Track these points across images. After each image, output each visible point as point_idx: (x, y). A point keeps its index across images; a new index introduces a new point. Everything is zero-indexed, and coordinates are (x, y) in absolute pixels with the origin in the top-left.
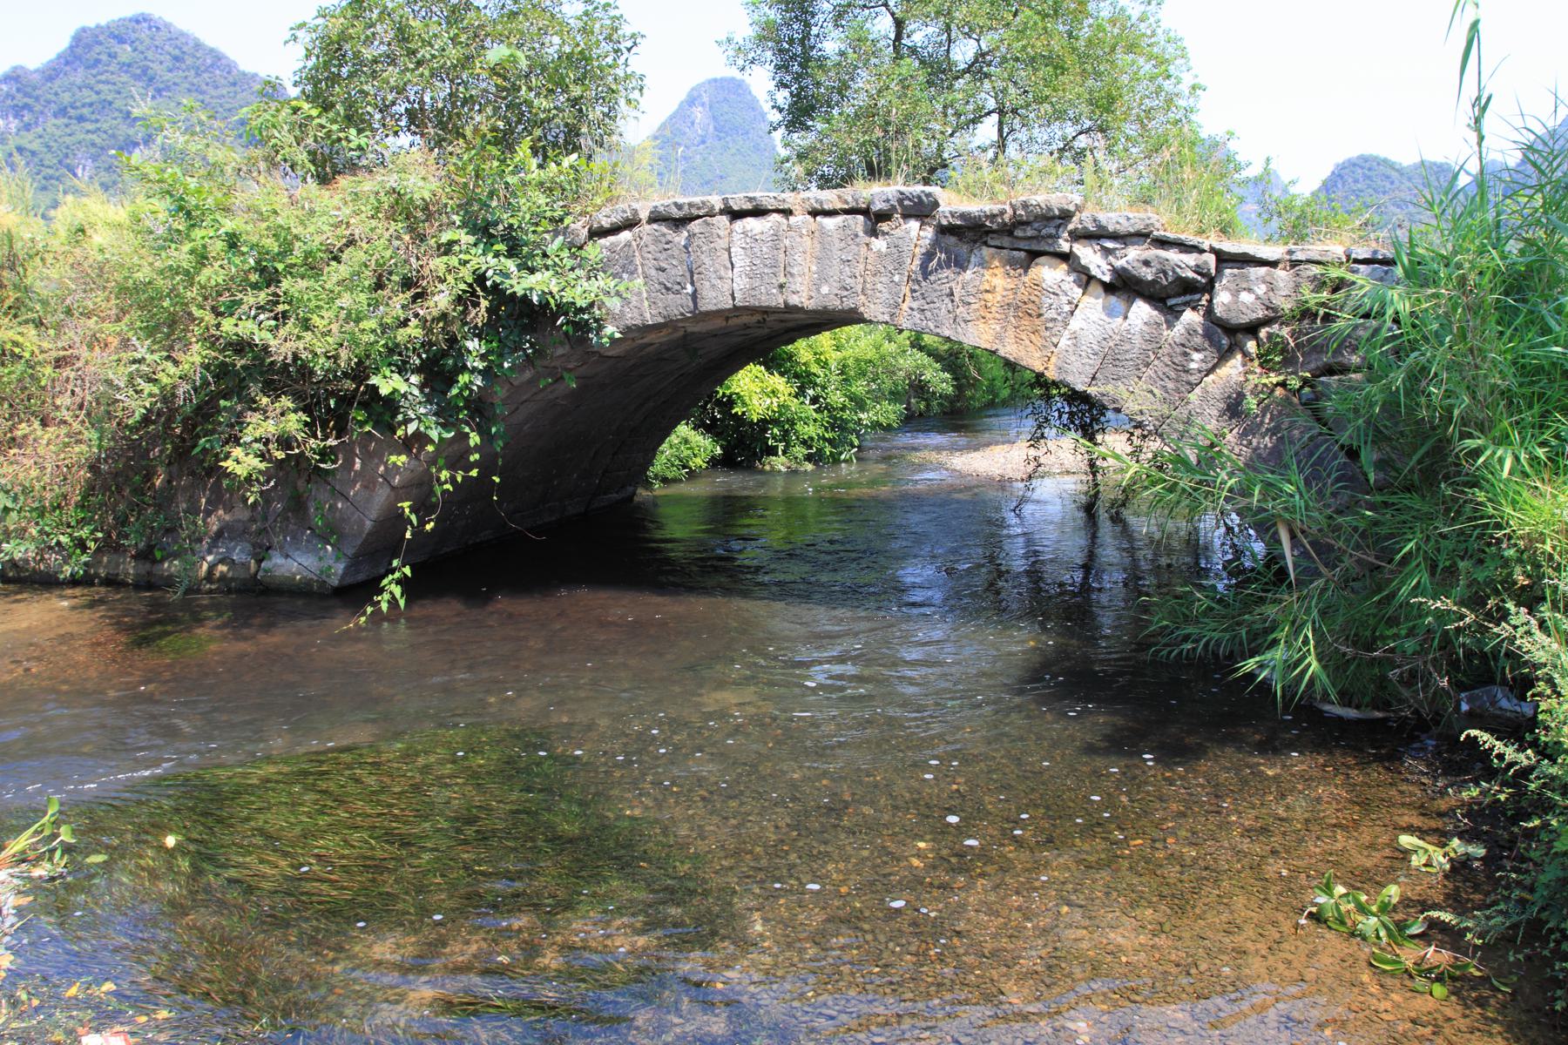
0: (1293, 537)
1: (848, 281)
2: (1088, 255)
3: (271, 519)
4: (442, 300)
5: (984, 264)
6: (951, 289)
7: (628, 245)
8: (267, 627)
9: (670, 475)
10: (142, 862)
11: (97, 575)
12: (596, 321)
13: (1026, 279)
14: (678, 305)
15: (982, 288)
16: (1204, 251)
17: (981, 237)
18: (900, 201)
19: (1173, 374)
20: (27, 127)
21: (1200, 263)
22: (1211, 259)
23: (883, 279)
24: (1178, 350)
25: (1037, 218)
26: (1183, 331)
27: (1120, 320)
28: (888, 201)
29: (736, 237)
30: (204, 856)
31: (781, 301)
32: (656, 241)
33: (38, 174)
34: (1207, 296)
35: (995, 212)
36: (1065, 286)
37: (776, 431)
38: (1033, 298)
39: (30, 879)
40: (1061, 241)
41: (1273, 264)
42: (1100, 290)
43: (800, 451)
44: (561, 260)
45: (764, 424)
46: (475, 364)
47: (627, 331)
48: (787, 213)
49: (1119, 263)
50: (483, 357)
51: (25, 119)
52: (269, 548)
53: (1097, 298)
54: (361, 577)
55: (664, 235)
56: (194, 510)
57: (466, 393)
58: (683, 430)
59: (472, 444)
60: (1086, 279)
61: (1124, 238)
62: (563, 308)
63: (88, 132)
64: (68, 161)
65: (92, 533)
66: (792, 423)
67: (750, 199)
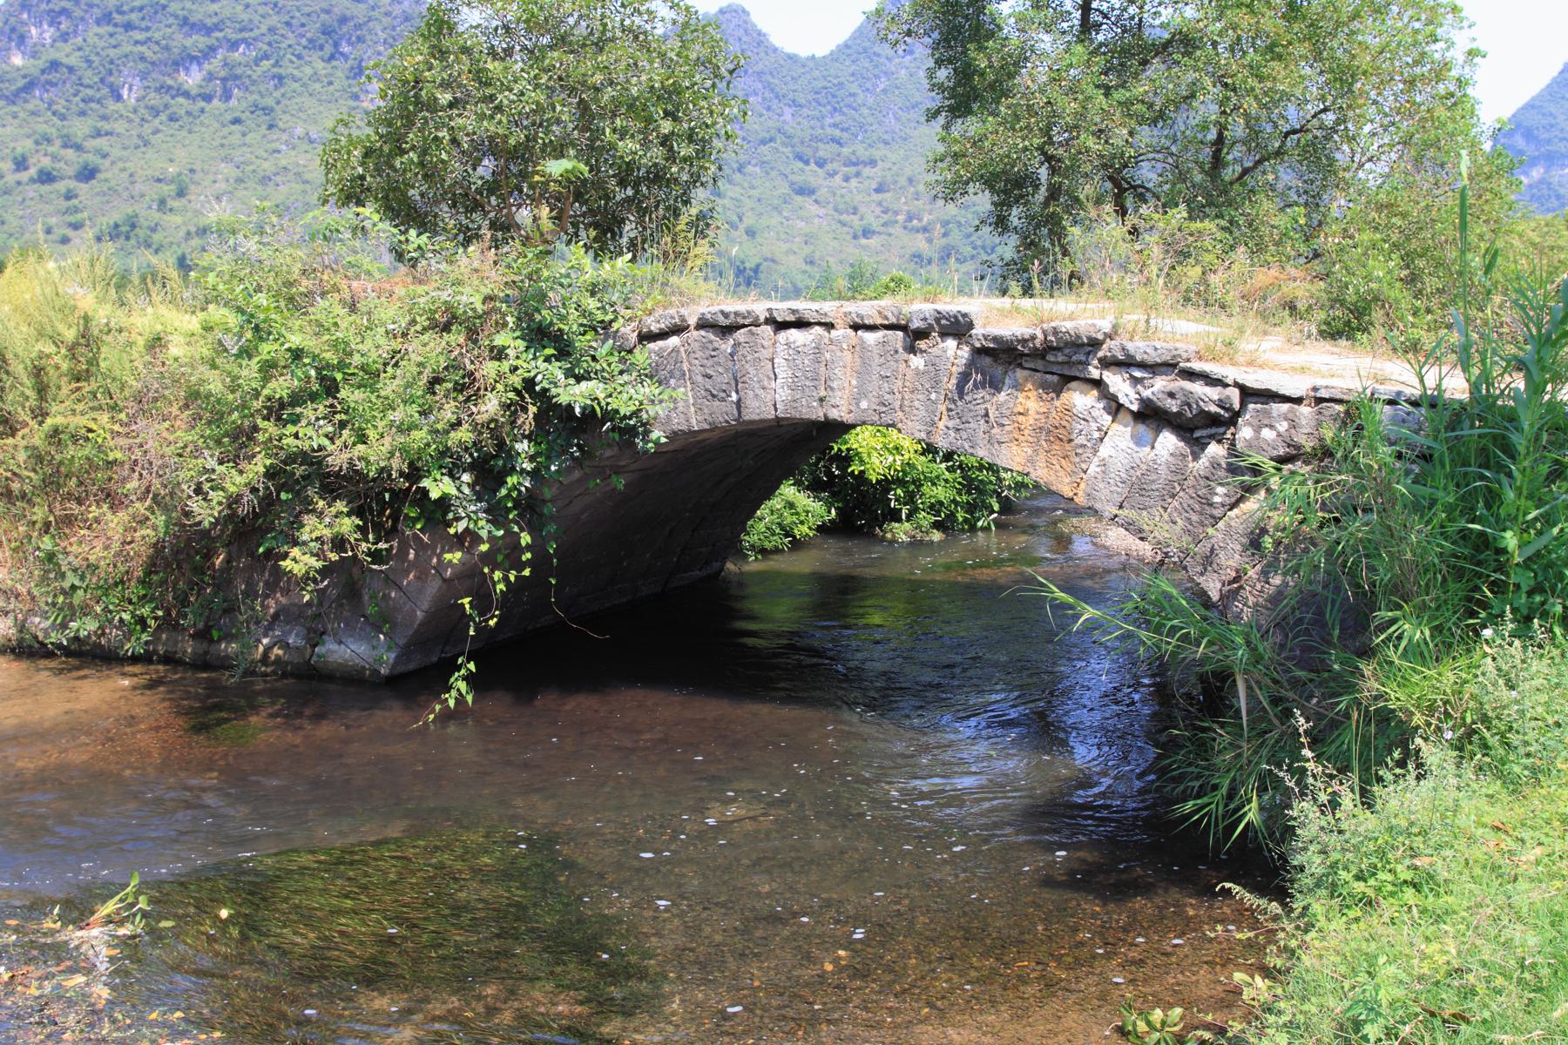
0: (1249, 688)
1: (887, 397)
2: (1117, 383)
3: (326, 605)
4: (490, 406)
5: (1018, 387)
6: (986, 409)
7: (675, 350)
8: (318, 717)
9: (768, 545)
10: (202, 929)
11: (155, 652)
12: (644, 425)
13: (1057, 403)
14: (722, 413)
15: (1015, 410)
16: (1229, 385)
17: (1015, 359)
18: (938, 320)
19: (1197, 507)
20: (65, 37)
21: (1223, 397)
22: (1234, 395)
23: (920, 397)
24: (1202, 482)
25: (1067, 344)
26: (1207, 464)
27: (1147, 449)
28: (925, 319)
29: (780, 348)
30: (249, 926)
31: (821, 414)
32: (704, 347)
33: (75, 95)
34: (1232, 430)
35: (1027, 337)
36: (1095, 413)
37: (899, 491)
38: (1064, 423)
39: (118, 937)
40: (1090, 368)
41: (1298, 401)
42: (1129, 418)
43: (925, 518)
44: (609, 365)
45: (886, 484)
46: (524, 466)
47: (674, 436)
48: (829, 326)
49: (1147, 393)
50: (532, 459)
51: (63, 27)
52: (323, 633)
53: (1126, 426)
54: (412, 666)
55: (711, 342)
56: (251, 593)
57: (515, 494)
58: (788, 490)
59: (523, 543)
60: (1115, 407)
61: (1154, 368)
62: (610, 415)
63: (137, 42)
64: (112, 79)
65: (153, 612)
66: (918, 483)
67: (794, 312)
